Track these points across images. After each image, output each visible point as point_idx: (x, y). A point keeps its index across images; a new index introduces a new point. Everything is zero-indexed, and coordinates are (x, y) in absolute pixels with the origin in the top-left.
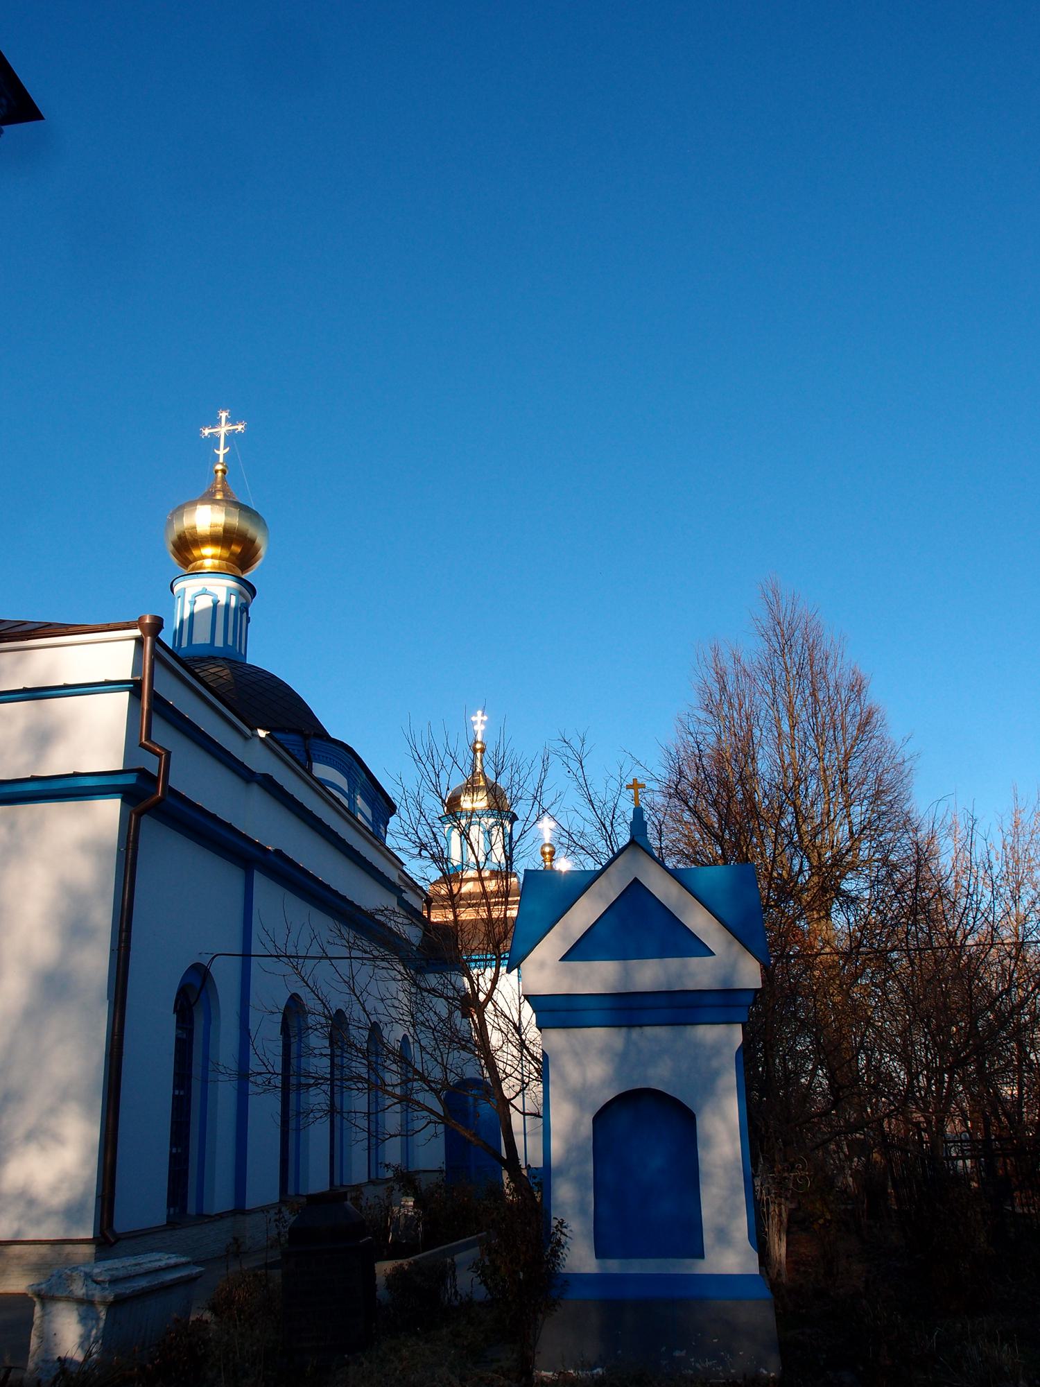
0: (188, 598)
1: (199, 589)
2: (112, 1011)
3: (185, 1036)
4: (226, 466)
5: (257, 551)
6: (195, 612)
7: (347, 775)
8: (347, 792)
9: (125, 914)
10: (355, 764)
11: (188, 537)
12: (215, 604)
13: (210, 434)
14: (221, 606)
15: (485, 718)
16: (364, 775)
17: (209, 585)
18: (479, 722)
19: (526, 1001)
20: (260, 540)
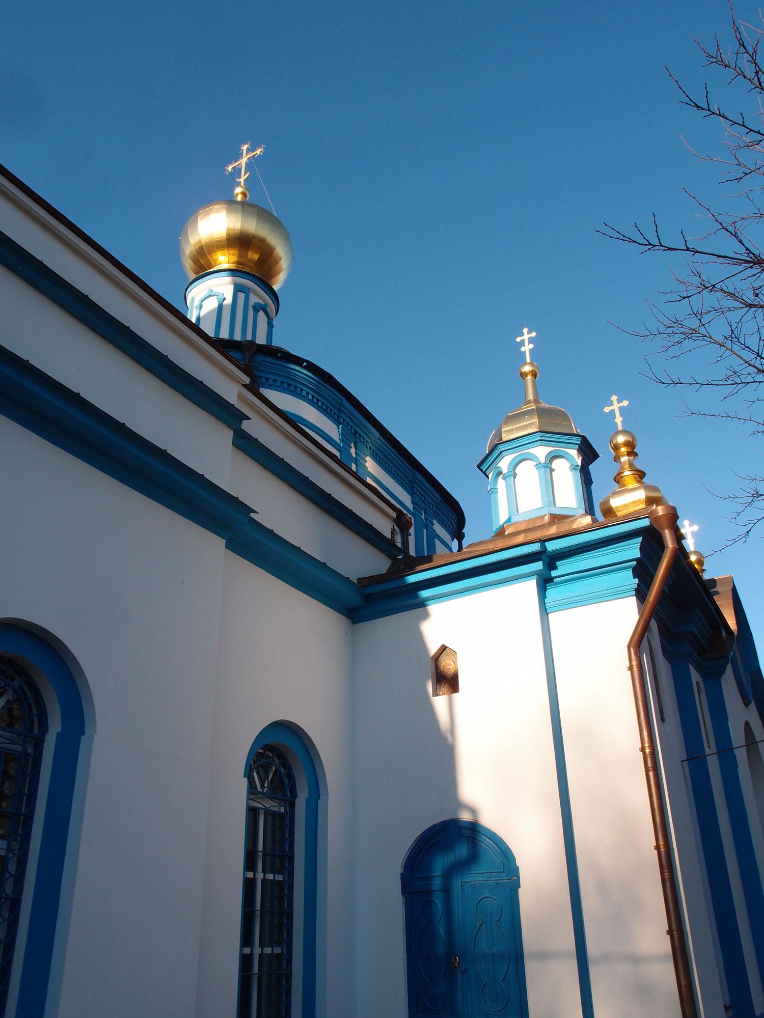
0: (196, 303)
1: (205, 293)
2: (665, 813)
3: (282, 810)
4: (247, 189)
5: (277, 261)
6: (201, 316)
7: (411, 492)
8: (412, 510)
9: (654, 791)
10: (345, 402)
11: (198, 249)
12: (220, 307)
13: (233, 168)
14: (227, 305)
15: (534, 334)
16: (376, 434)
17: (216, 286)
18: (526, 342)
19: (389, 536)
20: (281, 250)
